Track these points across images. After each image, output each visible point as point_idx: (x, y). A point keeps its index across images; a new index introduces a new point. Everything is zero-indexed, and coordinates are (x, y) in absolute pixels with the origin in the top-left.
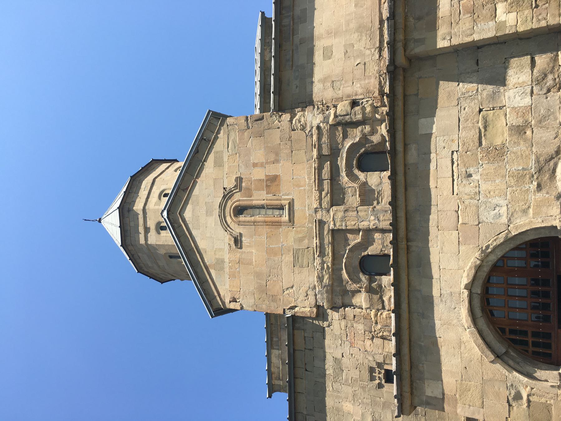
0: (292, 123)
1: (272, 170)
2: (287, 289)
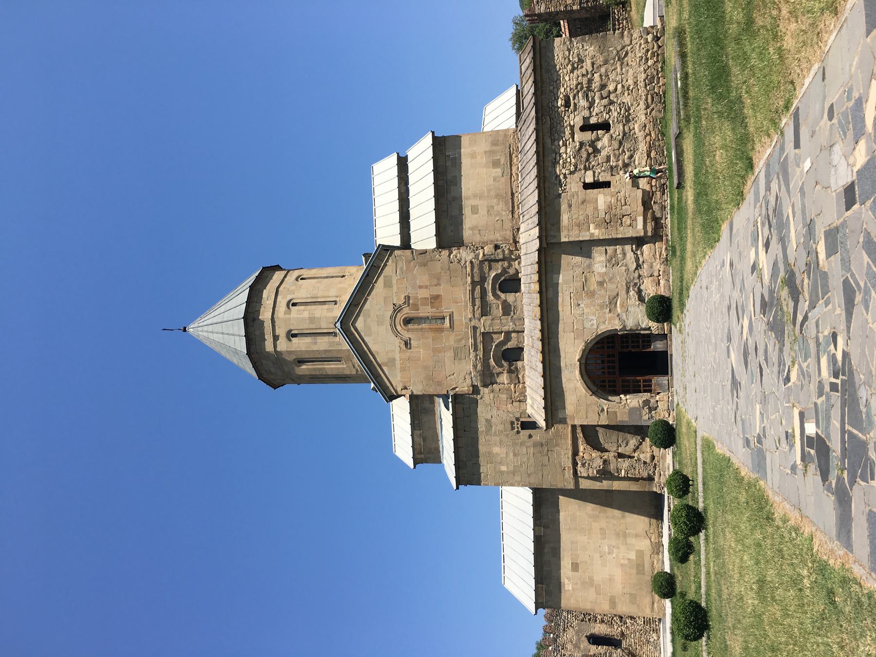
1: (435, 291)
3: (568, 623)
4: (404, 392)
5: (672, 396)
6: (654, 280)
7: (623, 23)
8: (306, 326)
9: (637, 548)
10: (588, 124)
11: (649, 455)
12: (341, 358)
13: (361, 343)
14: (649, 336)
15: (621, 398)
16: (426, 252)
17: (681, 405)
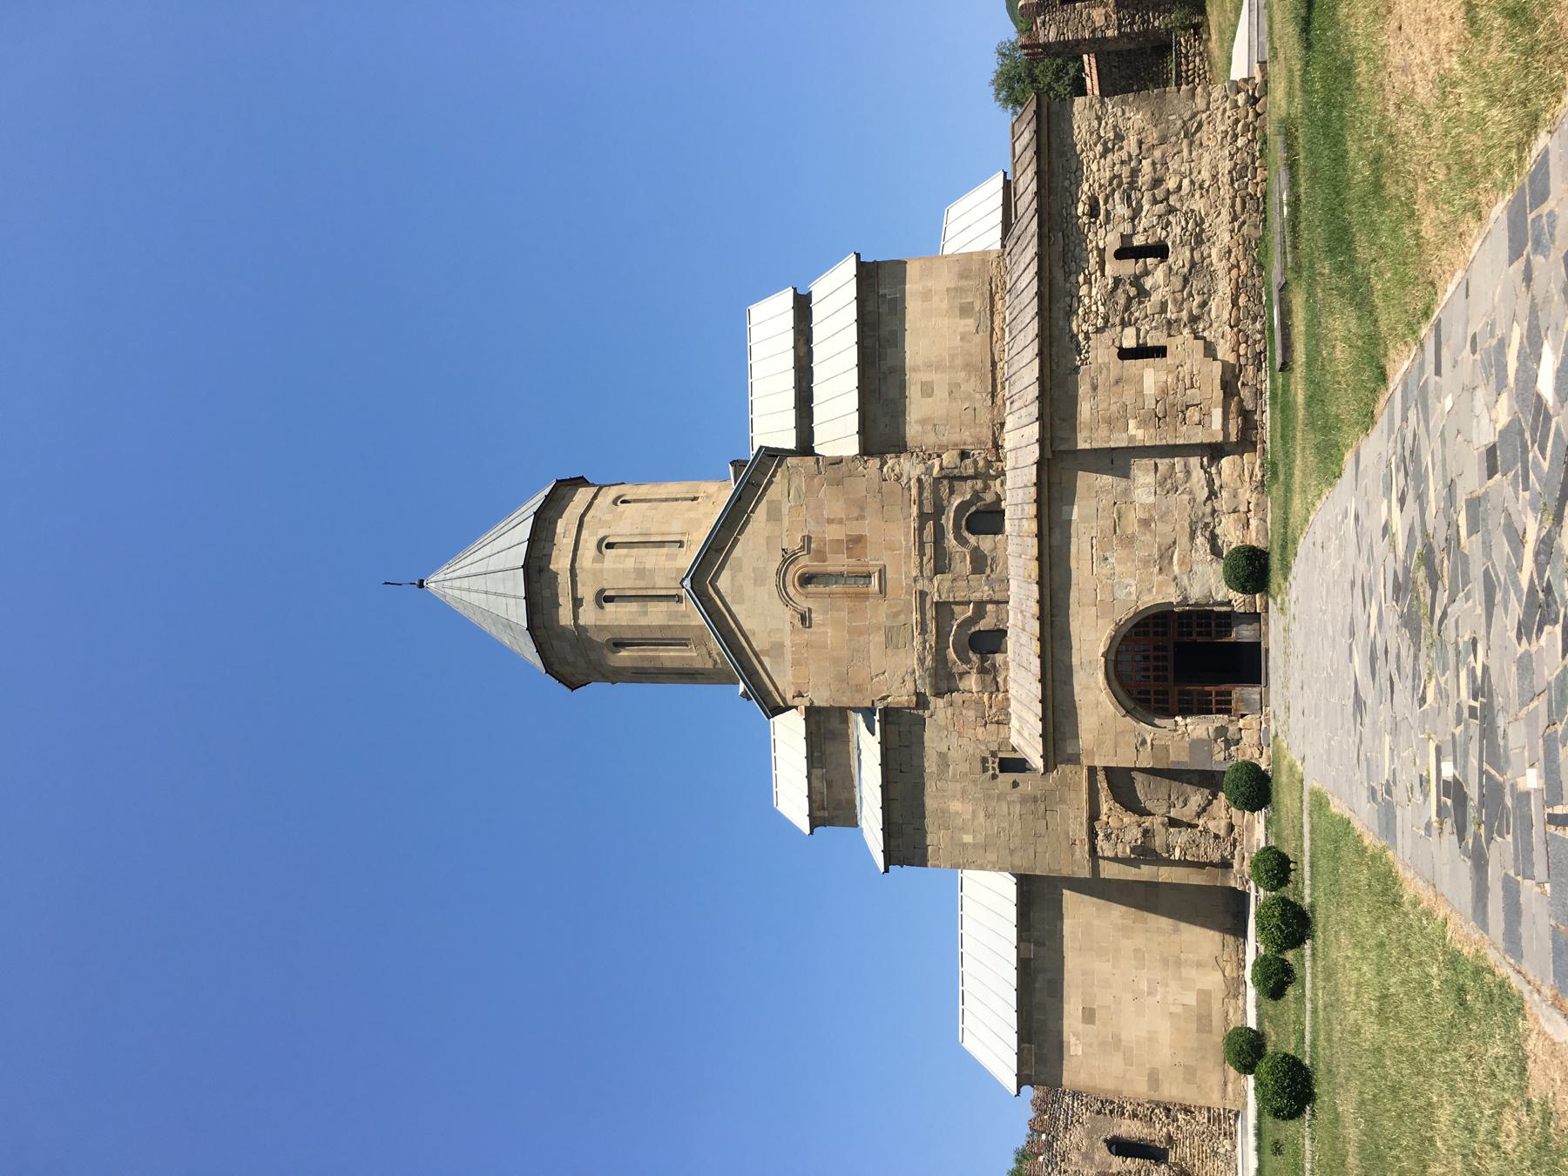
0: (882, 471)
1: (855, 529)
2: (877, 675)
3: (1072, 1116)
4: (797, 701)
5: (1268, 721)
6: (1240, 520)
7: (1194, 61)
8: (629, 584)
9: (1200, 986)
10: (1127, 246)
11: (1223, 823)
12: (689, 639)
13: (725, 616)
14: (1228, 615)
15: (1176, 722)
16: (841, 461)
17: (1281, 736)
